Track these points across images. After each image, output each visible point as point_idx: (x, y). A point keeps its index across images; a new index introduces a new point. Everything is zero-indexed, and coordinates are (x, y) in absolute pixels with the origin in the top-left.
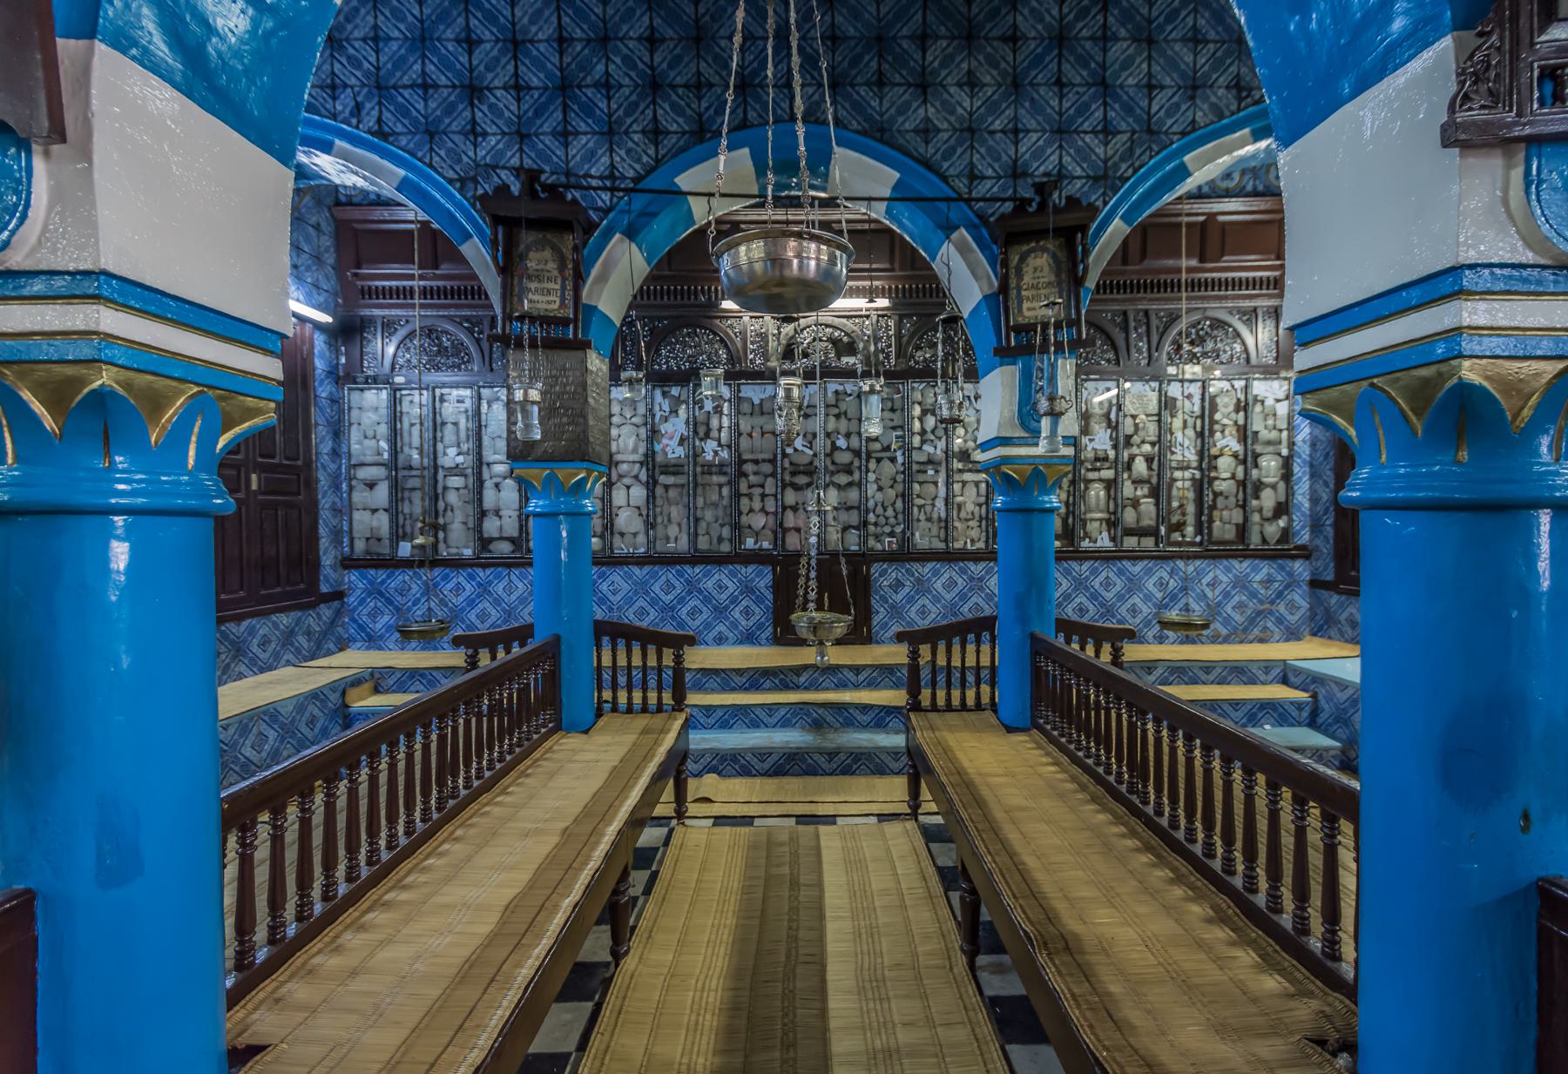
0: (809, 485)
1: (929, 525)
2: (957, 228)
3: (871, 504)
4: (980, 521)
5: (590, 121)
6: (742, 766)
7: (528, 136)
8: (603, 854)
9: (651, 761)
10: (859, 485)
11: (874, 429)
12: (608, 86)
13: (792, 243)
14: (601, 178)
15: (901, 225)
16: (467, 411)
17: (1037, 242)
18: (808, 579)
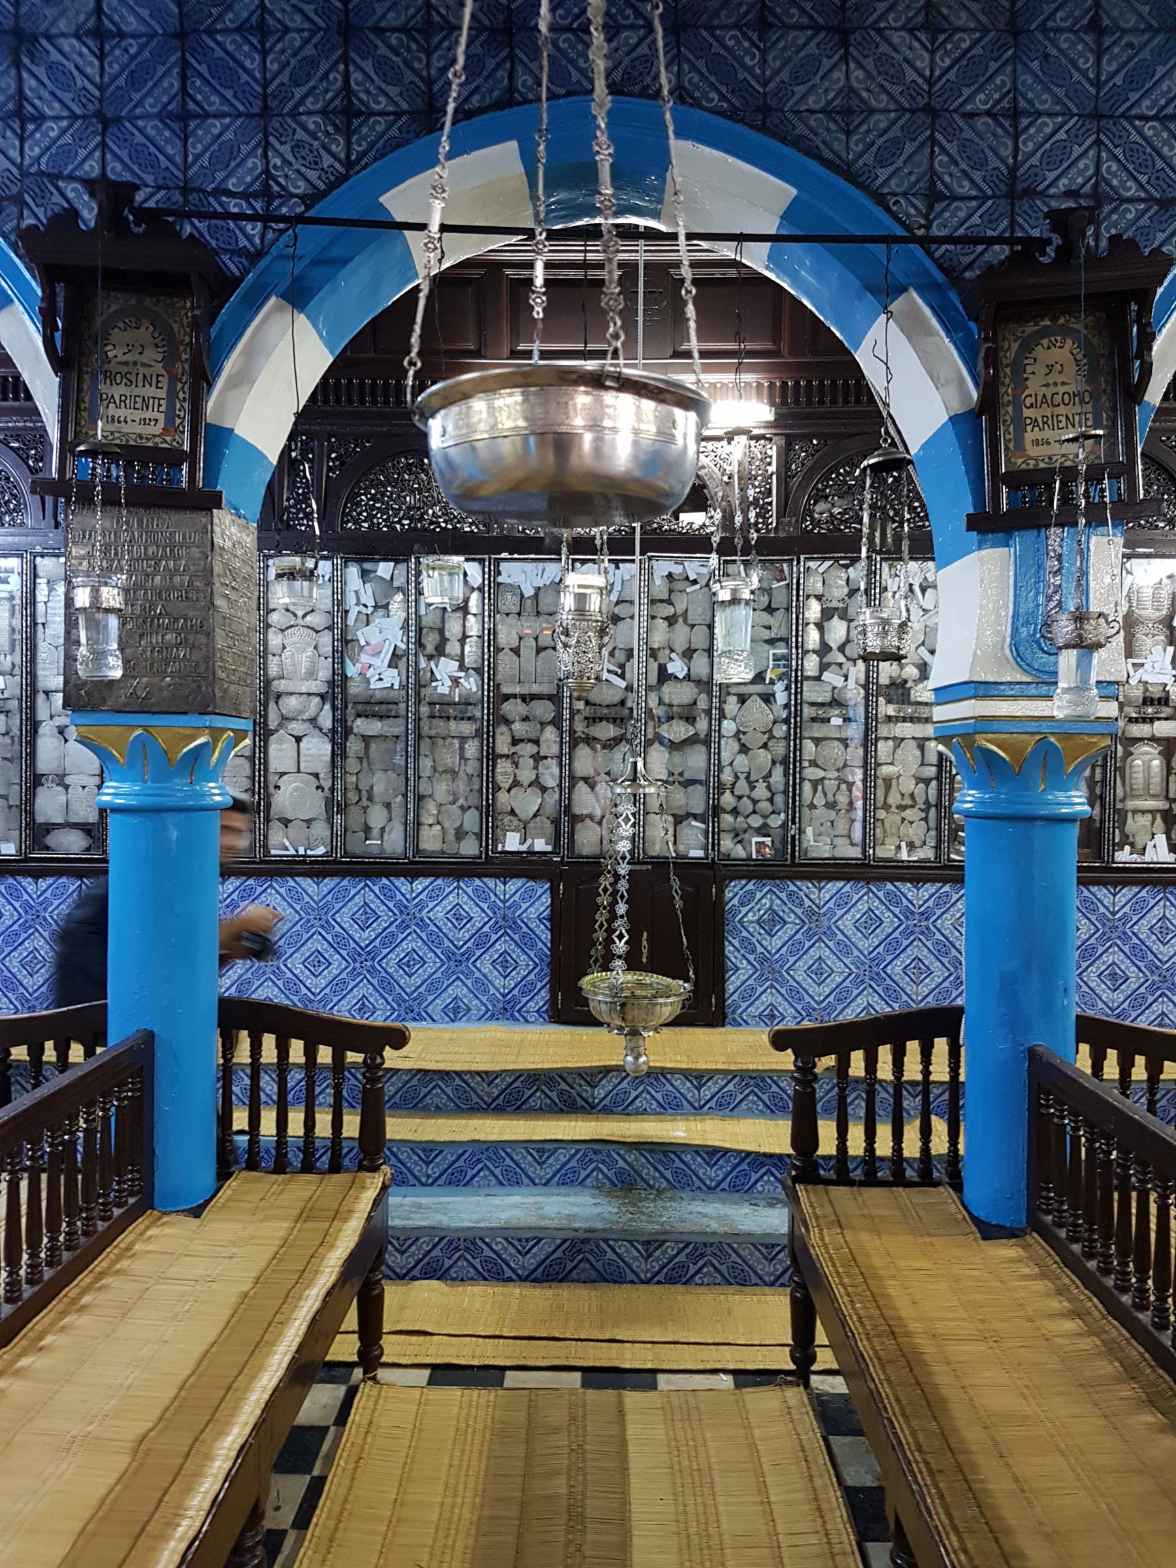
0: (617, 741)
1: (832, 814)
2: (903, 289)
3: (727, 777)
4: (926, 811)
5: (229, 94)
6: (486, 1261)
7: (118, 119)
8: (207, 1504)
9: (310, 1284)
10: (707, 742)
11: (736, 672)
12: (262, 30)
13: (582, 398)
14: (245, 195)
15: (795, 280)
16: (12, 598)
17: (1054, 319)
18: (613, 916)
